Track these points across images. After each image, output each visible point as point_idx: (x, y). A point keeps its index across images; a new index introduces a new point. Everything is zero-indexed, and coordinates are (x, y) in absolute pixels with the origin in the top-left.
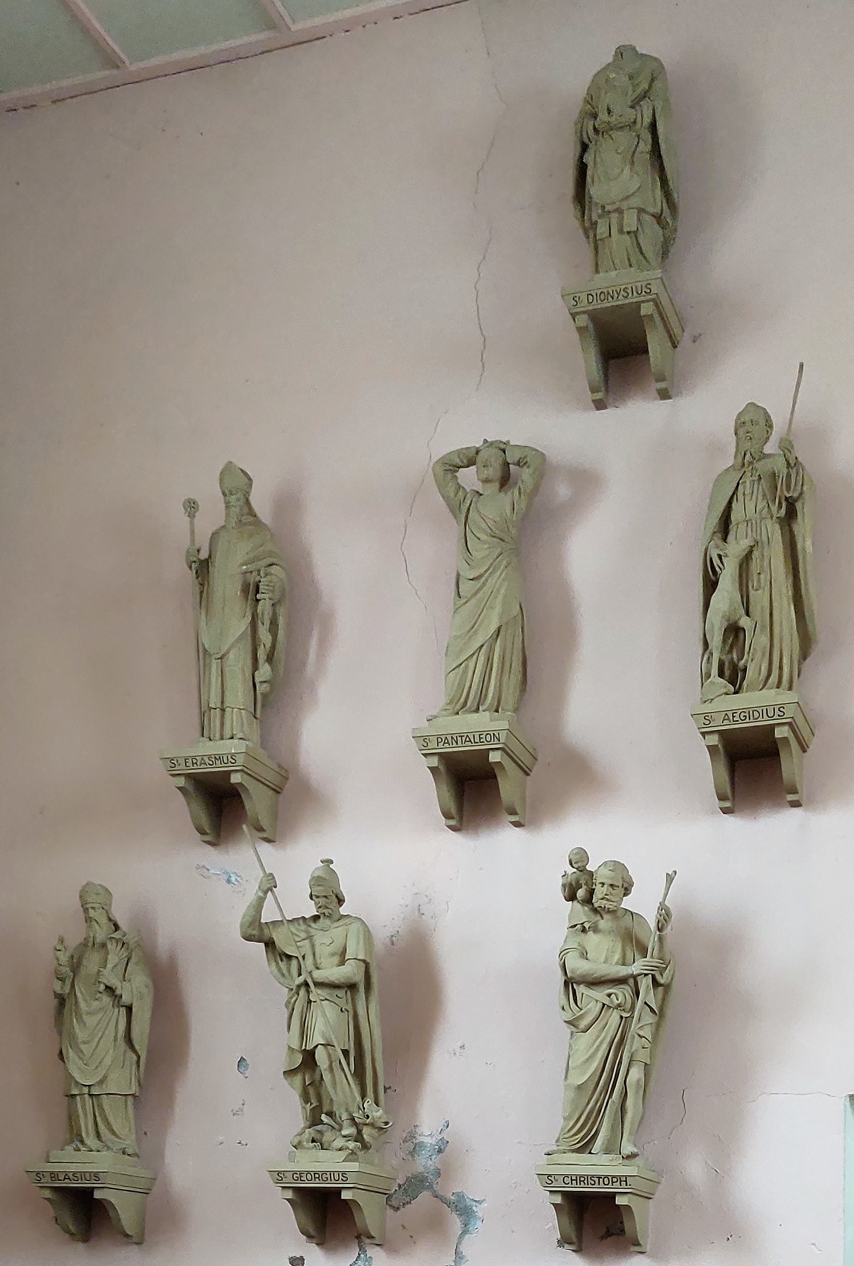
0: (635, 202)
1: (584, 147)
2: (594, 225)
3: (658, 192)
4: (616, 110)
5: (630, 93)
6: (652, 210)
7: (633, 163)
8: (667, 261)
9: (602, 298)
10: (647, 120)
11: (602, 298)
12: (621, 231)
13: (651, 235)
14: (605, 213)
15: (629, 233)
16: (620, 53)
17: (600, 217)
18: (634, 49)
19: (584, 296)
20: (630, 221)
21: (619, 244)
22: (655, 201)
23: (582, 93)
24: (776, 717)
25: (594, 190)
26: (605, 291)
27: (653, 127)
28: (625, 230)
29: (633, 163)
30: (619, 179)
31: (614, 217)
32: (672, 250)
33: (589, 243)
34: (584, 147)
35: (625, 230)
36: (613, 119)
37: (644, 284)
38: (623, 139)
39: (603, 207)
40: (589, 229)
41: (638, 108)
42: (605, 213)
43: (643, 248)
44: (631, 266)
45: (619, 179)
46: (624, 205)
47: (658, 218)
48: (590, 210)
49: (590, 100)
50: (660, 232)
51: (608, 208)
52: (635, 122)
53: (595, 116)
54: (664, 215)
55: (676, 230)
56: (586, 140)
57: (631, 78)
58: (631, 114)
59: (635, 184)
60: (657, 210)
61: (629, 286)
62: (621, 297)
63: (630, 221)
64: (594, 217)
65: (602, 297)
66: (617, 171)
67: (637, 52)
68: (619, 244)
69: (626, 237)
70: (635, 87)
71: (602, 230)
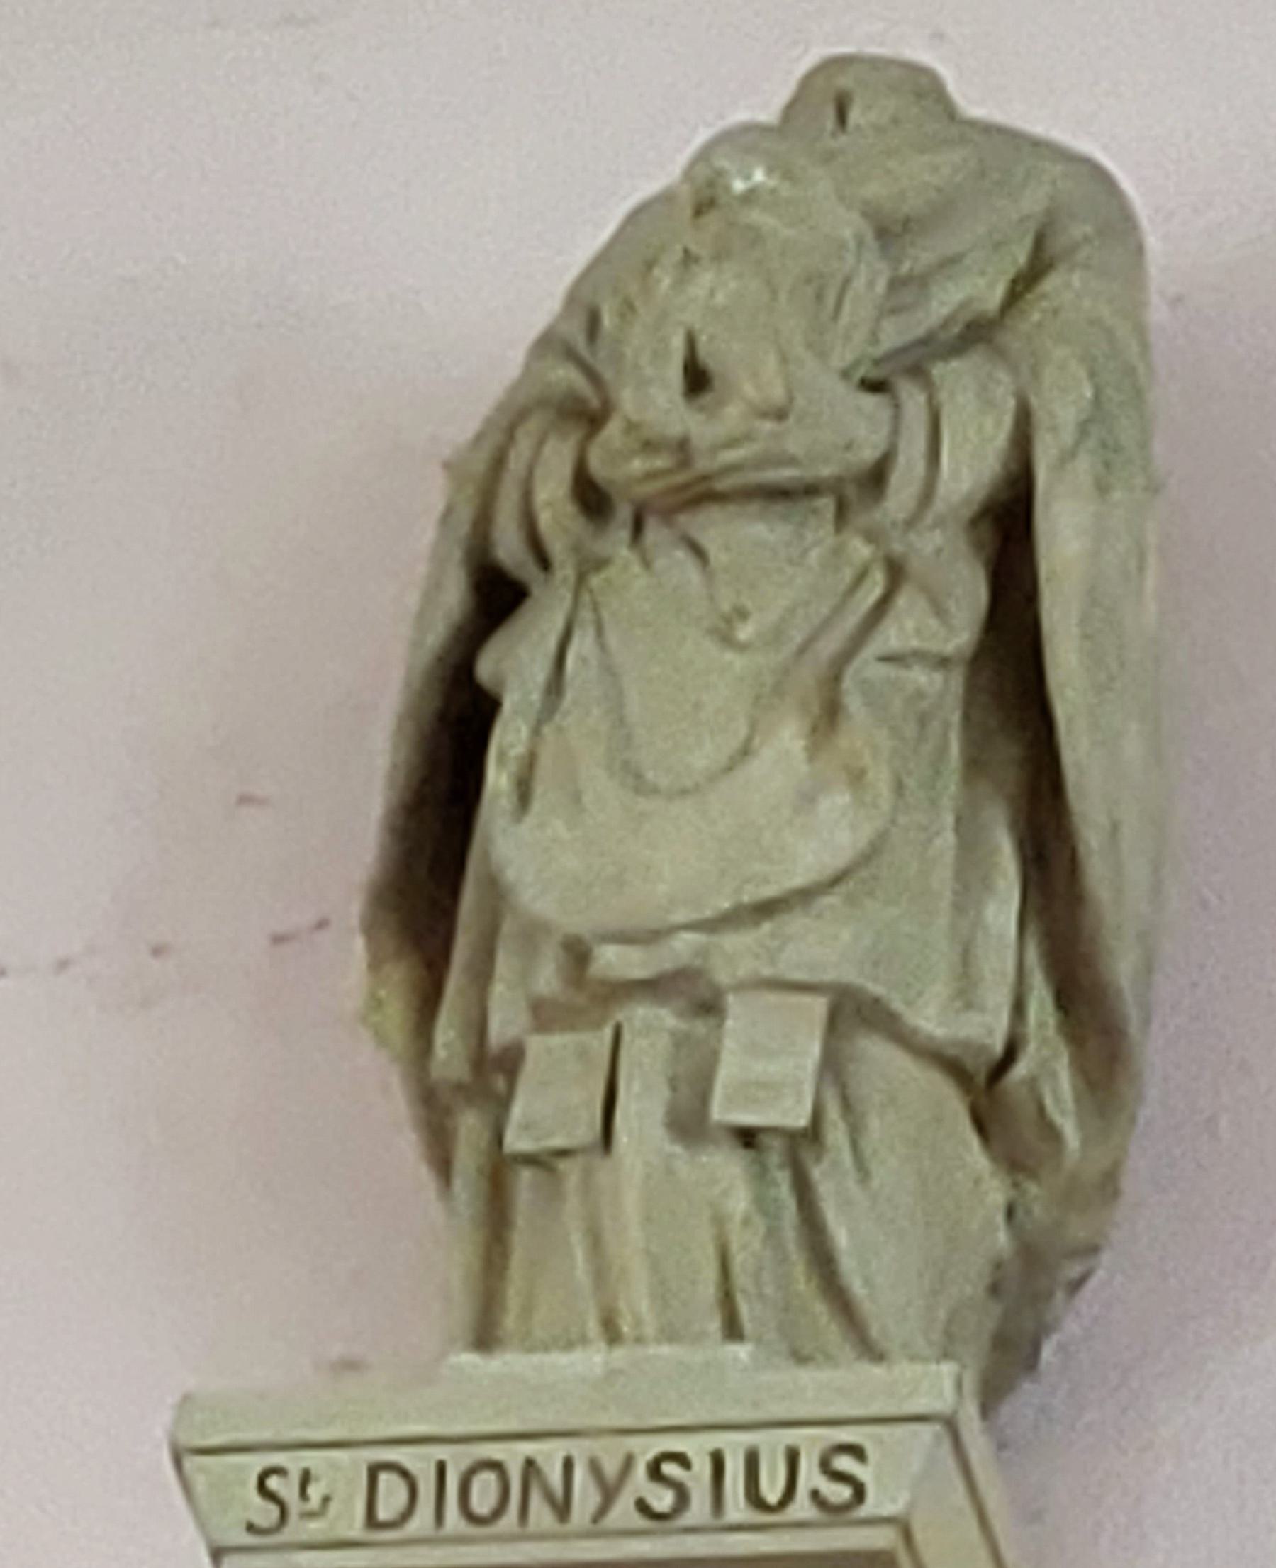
0: (824, 947)
1: (496, 597)
2: (496, 1070)
3: (1003, 908)
4: (752, 376)
5: (859, 307)
6: (931, 1019)
7: (829, 715)
8: (1027, 1394)
9: (482, 1501)
10: (970, 470)
11: (482, 1501)
12: (689, 1124)
13: (918, 1191)
14: (588, 995)
15: (747, 1137)
16: (831, 96)
17: (545, 1015)
18: (924, 88)
19: (340, 1475)
20: (769, 1066)
21: (662, 1200)
22: (968, 968)
23: (543, 306)
24: (801, 1508)
25: (524, 849)
26: (513, 1455)
27: (1008, 525)
28: (722, 1112)
29: (829, 715)
30: (719, 788)
31: (651, 1029)
32: (1073, 1327)
33: (443, 1165)
34: (496, 597)
35: (722, 1112)
36: (733, 415)
37: (811, 1442)
38: (777, 570)
39: (577, 954)
40: (459, 1102)
41: (913, 399)
42: (588, 995)
43: (848, 1266)
44: (733, 1330)
45: (719, 788)
46: (738, 955)
47: (985, 1086)
48: (483, 974)
49: (582, 331)
50: (996, 1193)
51: (613, 960)
52: (876, 478)
53: (588, 417)
54: (1021, 1070)
55: (1109, 1185)
56: (509, 548)
57: (889, 232)
58: (861, 427)
59: (828, 837)
60: (987, 1027)
61: (697, 1447)
62: (623, 1512)
63: (769, 1066)
64: (505, 1023)
65: (484, 1494)
66: (704, 757)
67: (950, 112)
68: (662, 1200)
69: (727, 1170)
70: (906, 289)
71: (547, 1107)
